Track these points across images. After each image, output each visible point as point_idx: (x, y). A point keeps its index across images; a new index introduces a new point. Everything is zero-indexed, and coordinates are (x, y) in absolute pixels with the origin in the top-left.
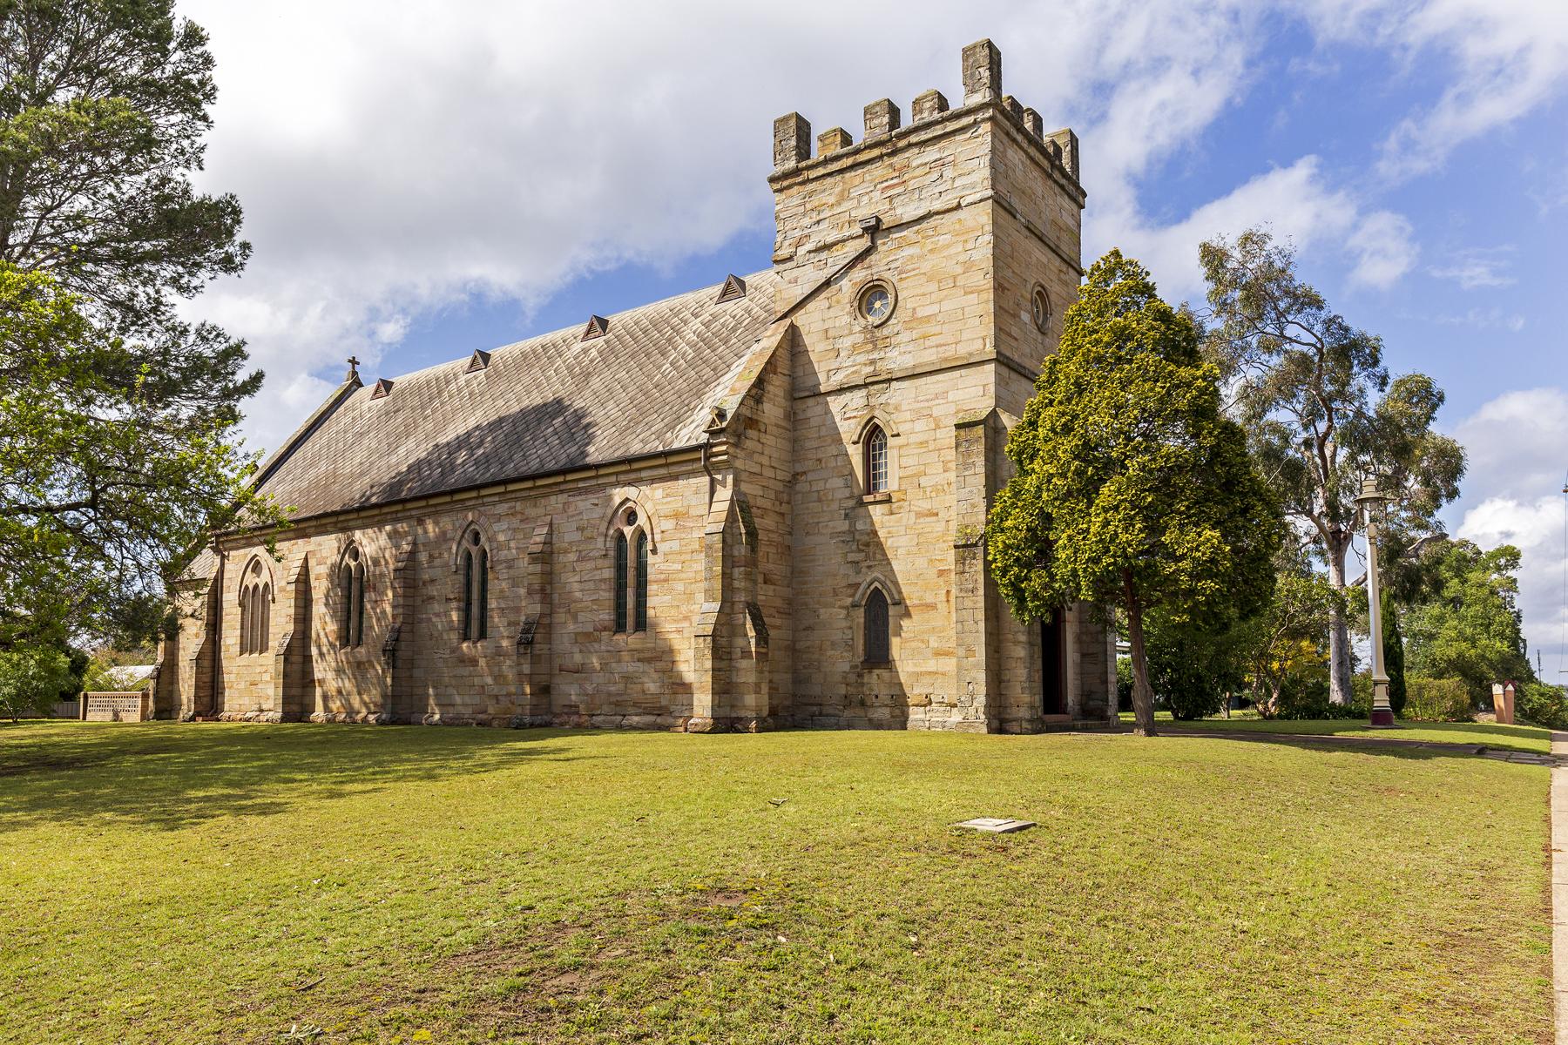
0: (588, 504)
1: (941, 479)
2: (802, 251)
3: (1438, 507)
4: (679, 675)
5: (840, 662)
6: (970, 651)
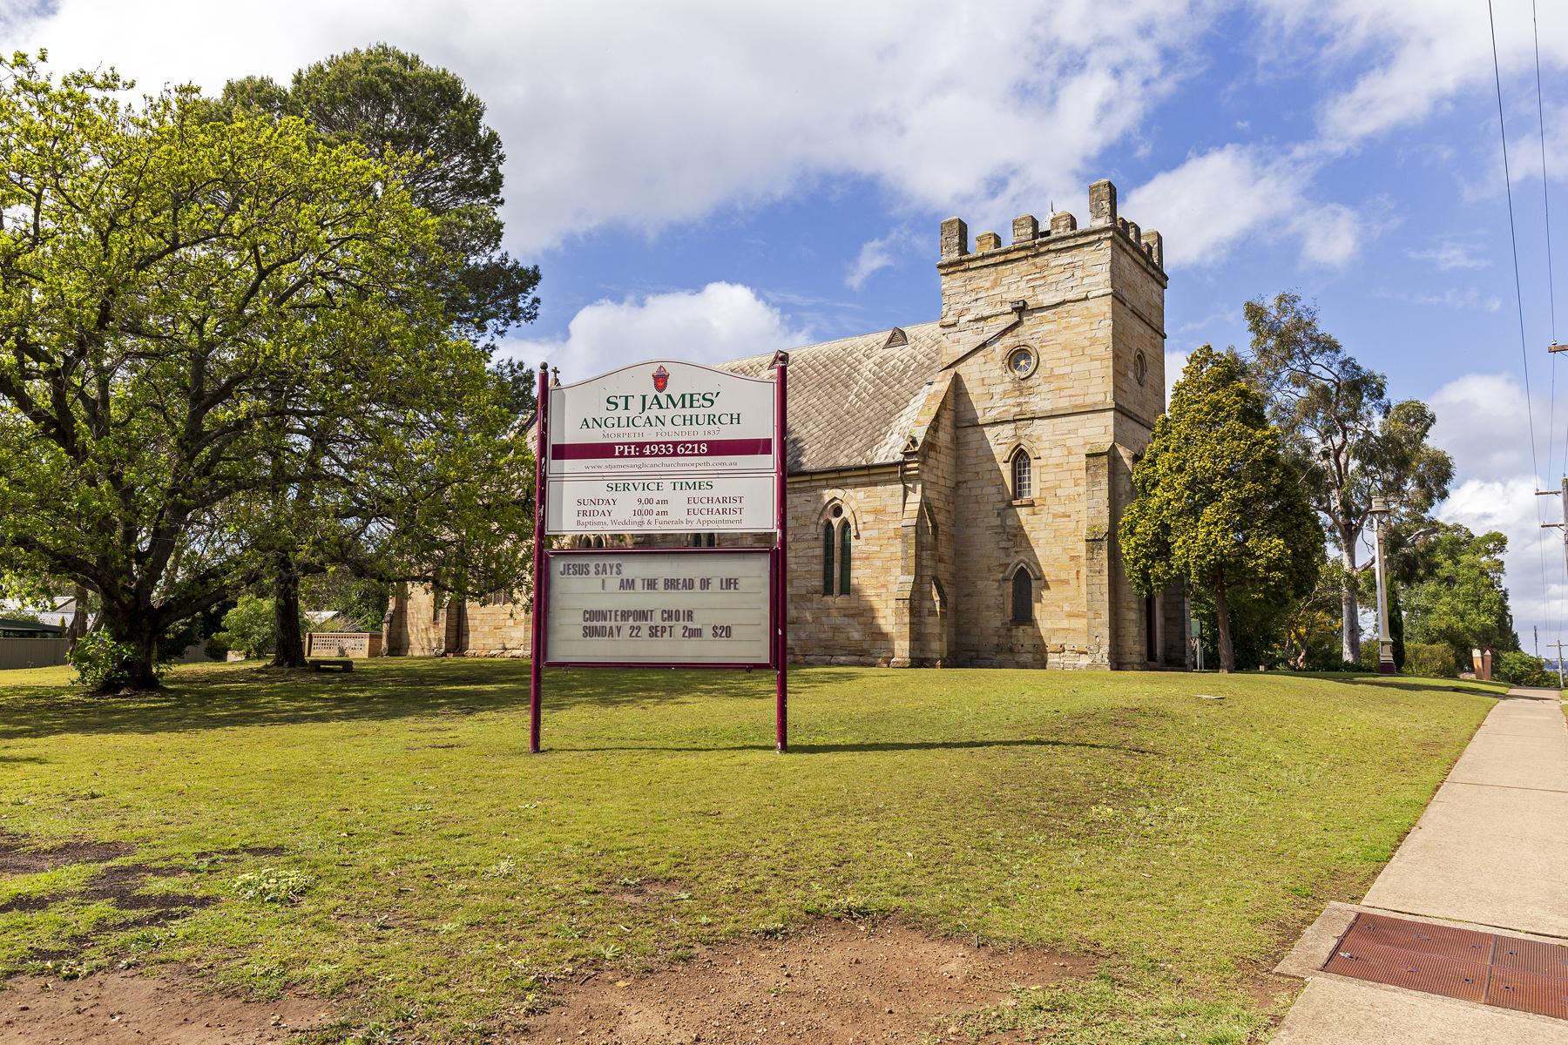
0: (802, 500)
1: (1073, 491)
2: (963, 320)
3: (1432, 505)
4: (878, 627)
5: (993, 619)
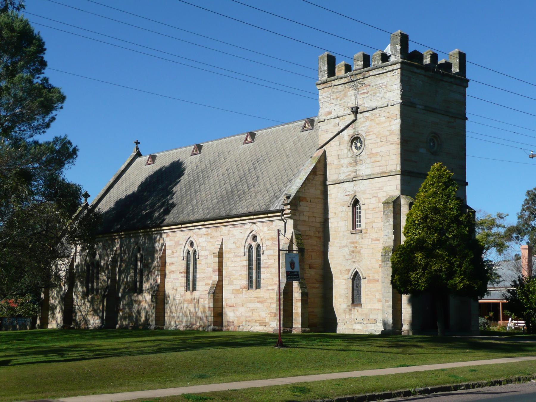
6: (387, 301)
